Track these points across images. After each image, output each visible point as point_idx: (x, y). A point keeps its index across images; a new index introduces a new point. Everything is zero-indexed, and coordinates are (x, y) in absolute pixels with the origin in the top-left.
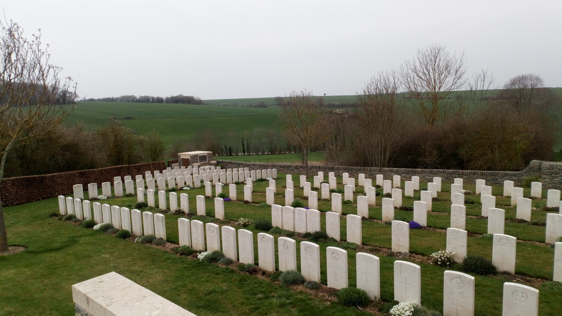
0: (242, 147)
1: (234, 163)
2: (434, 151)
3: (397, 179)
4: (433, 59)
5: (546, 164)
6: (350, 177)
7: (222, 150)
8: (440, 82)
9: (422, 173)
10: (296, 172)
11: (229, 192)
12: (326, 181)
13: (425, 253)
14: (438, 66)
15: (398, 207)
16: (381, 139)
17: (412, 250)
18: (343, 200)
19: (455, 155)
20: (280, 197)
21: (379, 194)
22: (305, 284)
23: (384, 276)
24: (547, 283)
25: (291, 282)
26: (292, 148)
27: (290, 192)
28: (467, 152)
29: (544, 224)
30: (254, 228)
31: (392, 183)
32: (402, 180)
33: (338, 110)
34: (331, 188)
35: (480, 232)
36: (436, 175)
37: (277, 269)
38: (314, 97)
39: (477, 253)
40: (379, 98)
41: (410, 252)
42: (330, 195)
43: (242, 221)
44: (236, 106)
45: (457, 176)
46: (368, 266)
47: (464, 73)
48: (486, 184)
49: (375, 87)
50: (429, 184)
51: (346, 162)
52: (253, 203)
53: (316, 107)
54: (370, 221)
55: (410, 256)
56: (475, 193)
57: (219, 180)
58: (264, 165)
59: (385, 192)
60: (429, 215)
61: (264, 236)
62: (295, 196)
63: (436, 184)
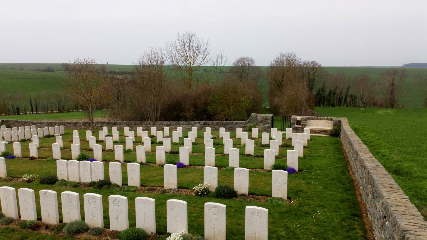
0: (30, 107)
1: (21, 122)
2: (192, 108)
3: (167, 129)
4: (188, 41)
5: (260, 115)
6: (130, 130)
7: (9, 110)
8: (194, 59)
9: (184, 125)
10: (82, 127)
11: (13, 150)
12: (110, 134)
13: (189, 187)
14: (192, 47)
15: (168, 151)
16: (154, 99)
17: (180, 186)
18: (124, 149)
19: (205, 111)
20: (66, 153)
21: (153, 143)
22: (89, 231)
23: (159, 211)
24: (269, 199)
25: (74, 232)
26: (79, 107)
27: (76, 148)
28: (213, 109)
29: (262, 156)
30: (39, 183)
31: (163, 133)
32: (170, 130)
33: (118, 77)
34: (114, 140)
35: (224, 166)
36: (193, 125)
37: (61, 221)
38: (97, 65)
39: (223, 182)
40: (151, 68)
41: (178, 188)
42: (114, 145)
43: (26, 177)
44: (22, 69)
45: (207, 126)
46: (145, 206)
47: (209, 53)
48: (226, 131)
49: (148, 59)
50: (189, 132)
51: (127, 118)
52: (39, 158)
53: (99, 73)
54: (147, 165)
55: (178, 191)
56: (219, 137)
57: (3, 138)
58: (51, 123)
59: (158, 140)
60: (191, 157)
61: (46, 193)
62: (81, 149)
63: (194, 132)
